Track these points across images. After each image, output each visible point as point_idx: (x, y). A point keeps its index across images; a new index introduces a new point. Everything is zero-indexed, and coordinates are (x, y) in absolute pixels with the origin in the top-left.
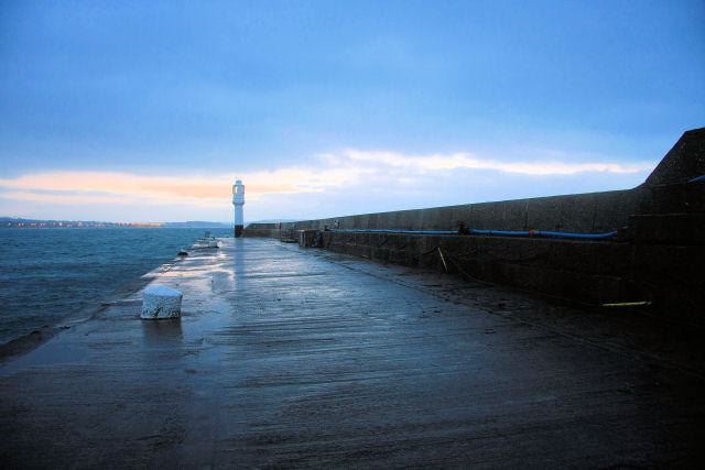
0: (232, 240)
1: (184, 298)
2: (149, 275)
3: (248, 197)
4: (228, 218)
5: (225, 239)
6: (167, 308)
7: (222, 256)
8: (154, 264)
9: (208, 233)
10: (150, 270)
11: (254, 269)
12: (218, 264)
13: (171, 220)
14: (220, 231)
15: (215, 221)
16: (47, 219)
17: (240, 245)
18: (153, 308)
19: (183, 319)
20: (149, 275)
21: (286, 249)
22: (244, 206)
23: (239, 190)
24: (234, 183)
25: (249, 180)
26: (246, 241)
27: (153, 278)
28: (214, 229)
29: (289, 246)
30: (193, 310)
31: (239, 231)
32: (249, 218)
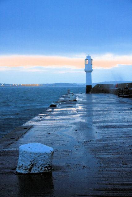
0: (85, 95)
1: (55, 155)
2: (29, 123)
3: (94, 67)
4: (81, 80)
5: (80, 95)
6: (40, 163)
7: (80, 108)
8: (33, 113)
9: (69, 92)
10: (27, 120)
11: (106, 119)
12: (76, 114)
13: (45, 83)
14: (75, 89)
15: (54, 83)
16: (46, 83)
17: (90, 99)
18: (27, 164)
19: (53, 173)
20: (29, 123)
21: (124, 103)
22: (92, 73)
23: (89, 61)
24: (86, 58)
25: (96, 58)
26: (94, 96)
27: (32, 127)
28: (73, 88)
29: (125, 100)
30: (62, 164)
31: (89, 89)
32: (96, 80)
